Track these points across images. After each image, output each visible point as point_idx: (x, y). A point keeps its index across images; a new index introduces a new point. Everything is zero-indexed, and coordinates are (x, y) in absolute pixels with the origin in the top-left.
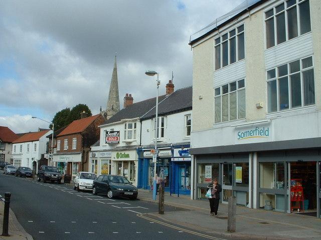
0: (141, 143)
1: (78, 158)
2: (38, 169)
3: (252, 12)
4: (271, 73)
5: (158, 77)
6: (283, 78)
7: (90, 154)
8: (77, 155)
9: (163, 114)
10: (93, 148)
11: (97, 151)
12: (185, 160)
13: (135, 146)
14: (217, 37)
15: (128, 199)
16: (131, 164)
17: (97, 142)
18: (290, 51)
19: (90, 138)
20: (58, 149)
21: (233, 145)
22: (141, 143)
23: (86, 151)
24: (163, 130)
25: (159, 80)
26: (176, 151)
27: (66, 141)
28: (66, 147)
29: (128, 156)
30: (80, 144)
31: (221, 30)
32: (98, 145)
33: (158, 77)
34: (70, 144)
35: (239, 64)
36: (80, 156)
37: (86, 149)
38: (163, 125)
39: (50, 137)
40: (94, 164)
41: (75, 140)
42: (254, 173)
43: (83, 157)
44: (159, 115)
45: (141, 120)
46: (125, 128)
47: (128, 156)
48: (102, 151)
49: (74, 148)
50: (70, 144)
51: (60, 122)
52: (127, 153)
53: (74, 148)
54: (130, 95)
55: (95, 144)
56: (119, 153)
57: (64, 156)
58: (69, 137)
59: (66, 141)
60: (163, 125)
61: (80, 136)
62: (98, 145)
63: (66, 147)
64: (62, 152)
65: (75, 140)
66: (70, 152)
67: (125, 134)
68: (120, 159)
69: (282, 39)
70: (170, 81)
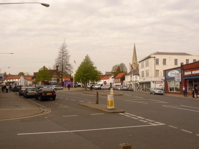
1: (120, 84)
6: (63, 132)
10: (124, 81)
12: (193, 73)
19: (123, 79)
20: (115, 81)
27: (117, 79)
28: (117, 81)
34: (118, 80)
36: (185, 74)
41: (119, 79)
42: (194, 77)
43: (121, 84)
49: (186, 73)
50: (118, 80)
53: (186, 73)
57: (196, 71)
59: (117, 79)
63: (117, 81)
64: (116, 82)
65: (119, 79)
66: (118, 82)
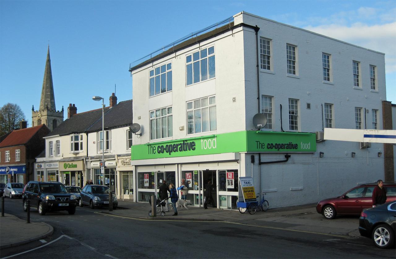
0: (87, 154)
3: (178, 53)
4: (189, 105)
5: (103, 102)
7: (36, 166)
8: (82, 168)
9: (108, 128)
10: (39, 160)
13: (81, 157)
14: (151, 69)
16: (78, 174)
17: (42, 153)
21: (389, 130)
22: (87, 154)
24: (107, 142)
26: (176, 149)
27: (8, 153)
29: (76, 166)
31: (155, 63)
32: (44, 156)
33: (103, 102)
44: (105, 129)
45: (87, 133)
47: (76, 166)
50: (13, 155)
51: (189, 201)
52: (74, 163)
54: (74, 105)
55: (40, 155)
56: (67, 163)
60: (107, 138)
61: (24, 148)
62: (44, 156)
65: (18, 152)
68: (68, 169)
69: (197, 80)
70: (114, 94)
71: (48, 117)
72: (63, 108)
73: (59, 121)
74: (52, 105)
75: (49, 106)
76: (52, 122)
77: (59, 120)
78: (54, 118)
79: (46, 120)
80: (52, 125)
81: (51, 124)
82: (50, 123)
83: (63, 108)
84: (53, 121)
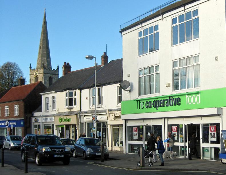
0: (81, 109)
2: (131, 153)
4: (175, 63)
5: (95, 60)
7: (33, 120)
9: (100, 85)
10: (36, 114)
11: (40, 116)
14: (140, 30)
15: (62, 163)
16: (73, 127)
17: (39, 108)
18: (186, 49)
22: (81, 109)
23: (28, 117)
25: (97, 63)
27: (7, 108)
29: (70, 120)
30: (23, 111)
31: (143, 24)
32: (40, 110)
33: (95, 60)
35: (154, 54)
37: (29, 115)
38: (99, 94)
39: (56, 129)
40: (37, 129)
44: (97, 86)
45: (81, 90)
46: (66, 96)
47: (70, 120)
48: (44, 117)
50: (12, 110)
52: (69, 117)
54: (68, 63)
55: (37, 110)
58: (10, 103)
60: (99, 94)
61: (22, 103)
62: (40, 110)
65: (16, 107)
67: (43, 79)
68: (63, 123)
69: (182, 41)
70: (105, 53)
71: (45, 74)
72: (58, 67)
73: (54, 79)
74: (48, 64)
75: (46, 65)
76: (48, 79)
77: (55, 77)
78: (50, 75)
79: (43, 77)
80: (48, 82)
81: (47, 81)
82: (46, 81)
83: (58, 67)
84: (49, 78)
